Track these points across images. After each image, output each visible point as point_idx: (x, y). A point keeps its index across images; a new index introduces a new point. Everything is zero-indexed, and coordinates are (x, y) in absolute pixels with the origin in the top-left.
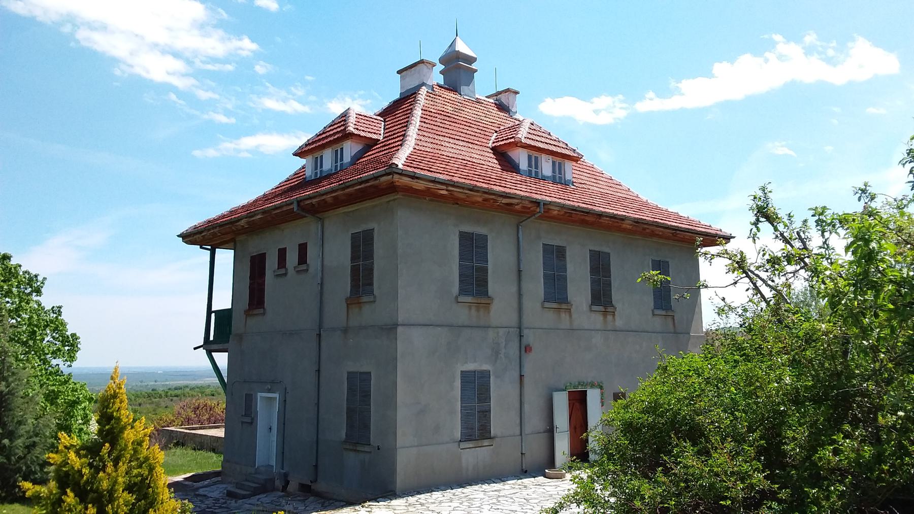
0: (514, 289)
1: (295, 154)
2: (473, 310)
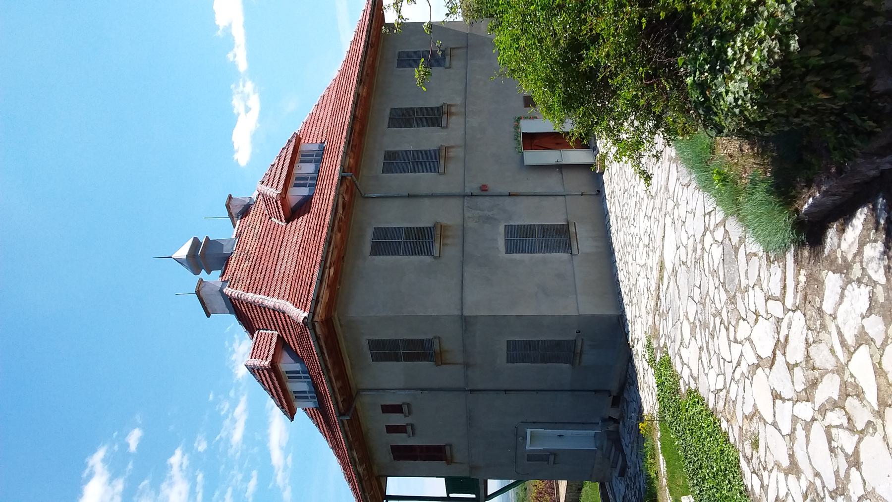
0: (427, 201)
1: (292, 419)
2: (448, 241)
